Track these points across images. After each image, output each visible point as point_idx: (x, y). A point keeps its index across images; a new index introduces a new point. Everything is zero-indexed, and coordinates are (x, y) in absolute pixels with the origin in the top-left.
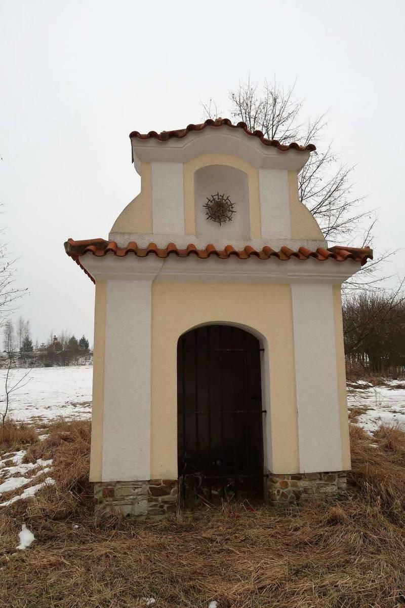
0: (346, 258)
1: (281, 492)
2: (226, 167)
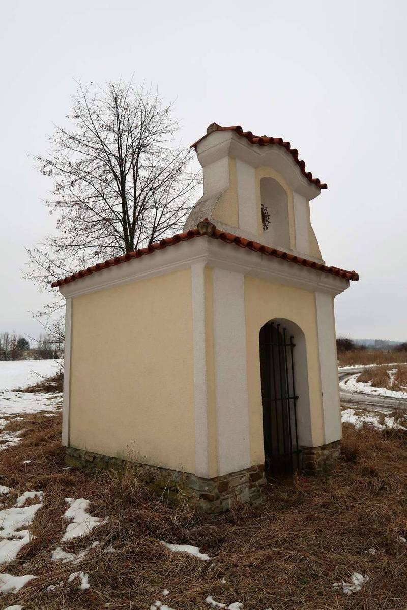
0: (245, 246)
2: (286, 194)
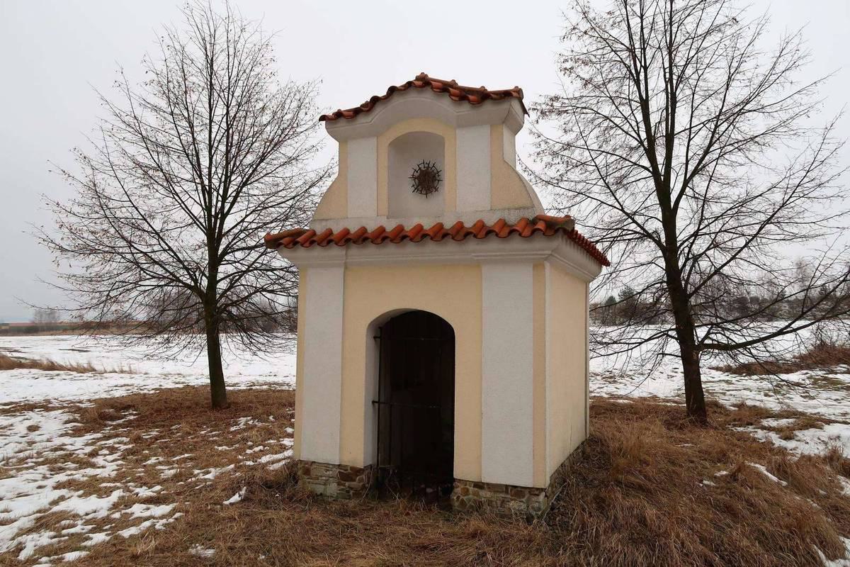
1: (461, 498)
